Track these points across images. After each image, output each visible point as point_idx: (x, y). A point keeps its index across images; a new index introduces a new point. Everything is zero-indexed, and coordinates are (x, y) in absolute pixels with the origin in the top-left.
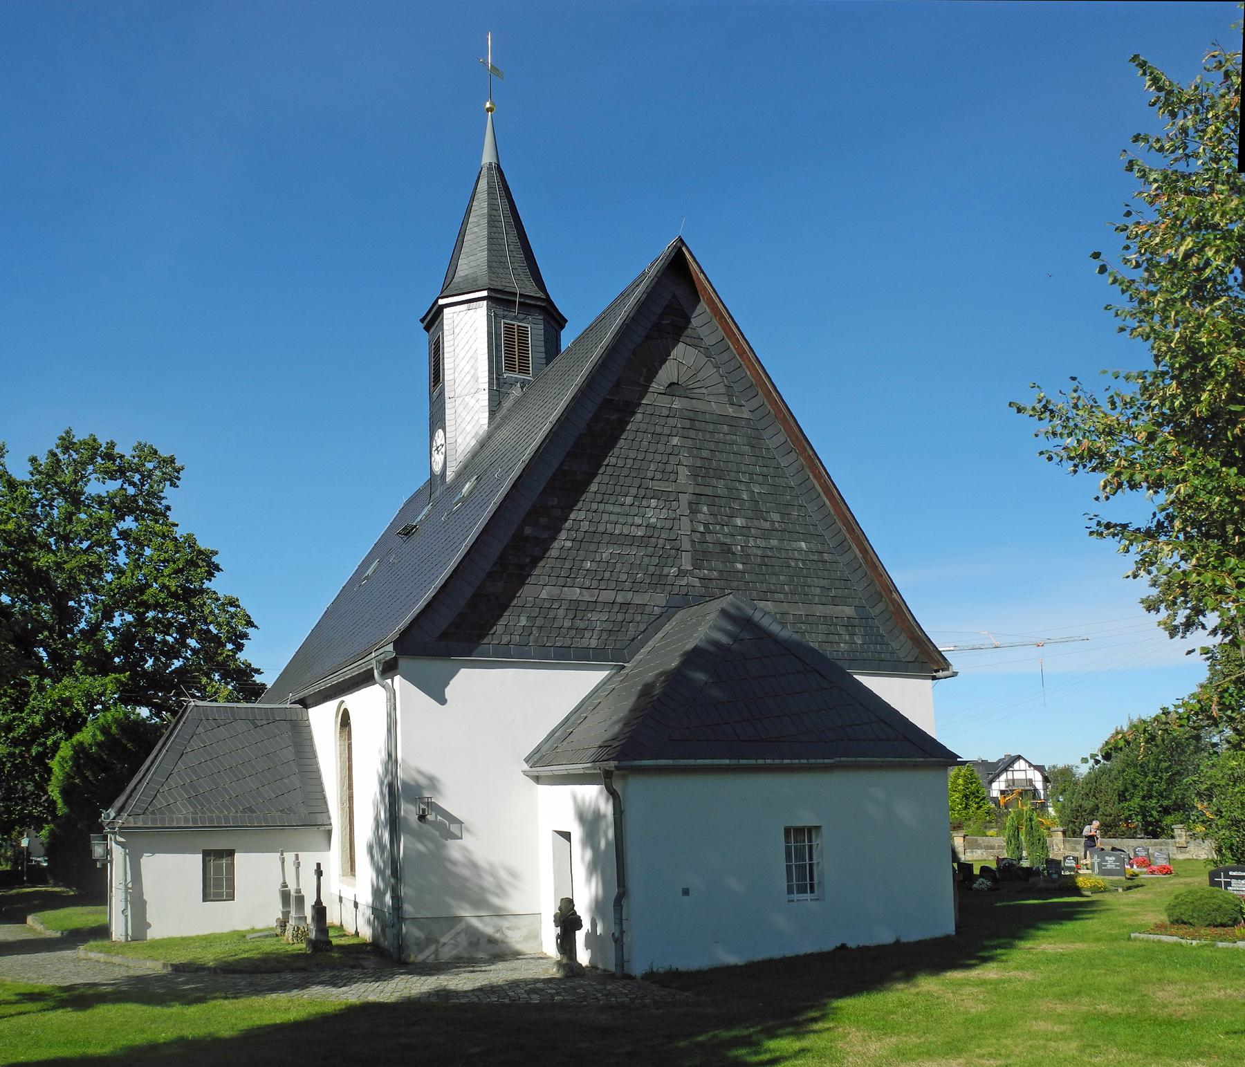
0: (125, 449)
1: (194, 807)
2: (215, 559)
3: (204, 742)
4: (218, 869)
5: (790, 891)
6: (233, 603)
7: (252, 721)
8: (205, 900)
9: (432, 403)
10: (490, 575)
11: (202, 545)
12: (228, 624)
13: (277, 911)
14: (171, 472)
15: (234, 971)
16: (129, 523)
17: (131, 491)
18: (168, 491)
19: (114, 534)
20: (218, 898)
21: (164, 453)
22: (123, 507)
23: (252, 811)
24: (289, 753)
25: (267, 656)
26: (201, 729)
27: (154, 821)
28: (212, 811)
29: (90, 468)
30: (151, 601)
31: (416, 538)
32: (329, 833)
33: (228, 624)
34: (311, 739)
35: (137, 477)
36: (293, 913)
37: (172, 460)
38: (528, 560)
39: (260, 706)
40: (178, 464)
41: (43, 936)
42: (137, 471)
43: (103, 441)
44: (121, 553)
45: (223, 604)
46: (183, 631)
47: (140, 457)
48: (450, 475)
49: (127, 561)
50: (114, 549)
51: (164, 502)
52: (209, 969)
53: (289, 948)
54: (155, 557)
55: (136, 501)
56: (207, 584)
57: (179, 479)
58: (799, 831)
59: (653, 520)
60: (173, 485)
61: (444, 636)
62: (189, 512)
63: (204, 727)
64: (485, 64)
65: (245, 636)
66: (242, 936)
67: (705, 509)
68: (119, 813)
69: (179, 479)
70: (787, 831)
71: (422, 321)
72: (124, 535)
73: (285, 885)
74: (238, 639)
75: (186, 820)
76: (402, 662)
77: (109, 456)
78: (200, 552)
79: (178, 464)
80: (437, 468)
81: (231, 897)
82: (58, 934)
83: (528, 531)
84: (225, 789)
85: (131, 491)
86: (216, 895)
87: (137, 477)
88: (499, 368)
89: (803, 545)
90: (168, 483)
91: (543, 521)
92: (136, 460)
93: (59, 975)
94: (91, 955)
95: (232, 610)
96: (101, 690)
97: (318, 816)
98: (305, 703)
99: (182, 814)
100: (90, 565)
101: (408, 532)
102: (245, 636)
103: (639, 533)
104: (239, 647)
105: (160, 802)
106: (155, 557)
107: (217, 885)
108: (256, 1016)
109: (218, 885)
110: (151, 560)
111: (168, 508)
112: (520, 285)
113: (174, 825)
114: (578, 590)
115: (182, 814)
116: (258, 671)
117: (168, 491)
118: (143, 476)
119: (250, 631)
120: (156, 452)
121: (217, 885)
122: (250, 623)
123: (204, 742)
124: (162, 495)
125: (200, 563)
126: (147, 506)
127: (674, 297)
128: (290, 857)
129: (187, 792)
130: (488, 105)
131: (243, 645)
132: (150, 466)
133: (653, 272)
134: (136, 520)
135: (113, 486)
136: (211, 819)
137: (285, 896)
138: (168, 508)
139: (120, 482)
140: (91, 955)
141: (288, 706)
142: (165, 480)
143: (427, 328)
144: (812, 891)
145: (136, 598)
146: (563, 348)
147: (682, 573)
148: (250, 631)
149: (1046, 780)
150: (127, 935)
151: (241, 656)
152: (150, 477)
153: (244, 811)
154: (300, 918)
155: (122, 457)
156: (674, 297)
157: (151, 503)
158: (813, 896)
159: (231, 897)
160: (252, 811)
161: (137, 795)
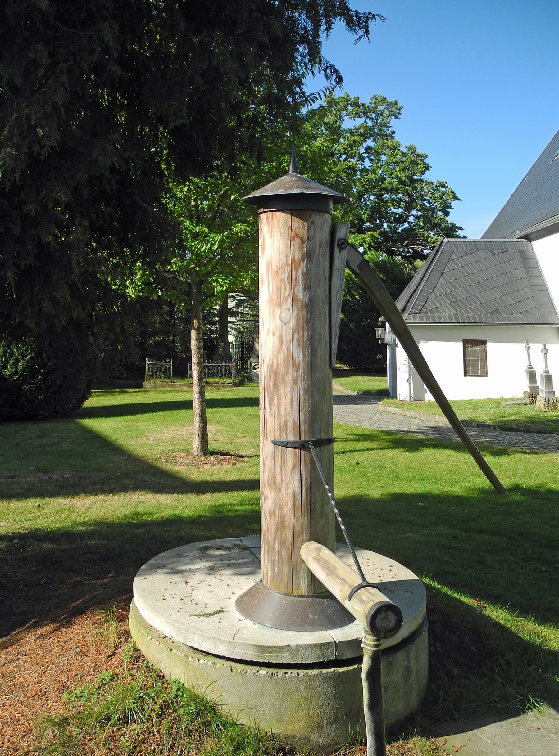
0: (366, 100)
1: (455, 309)
2: (426, 161)
3: (456, 264)
4: (475, 354)
6: (443, 185)
7: (491, 251)
8: (465, 375)
11: (419, 151)
12: (441, 198)
13: (525, 386)
14: (395, 110)
15: (511, 430)
16: (370, 143)
17: (370, 123)
18: (393, 122)
19: (362, 150)
21: (390, 99)
22: (366, 134)
23: (499, 313)
24: (520, 273)
26: (454, 256)
27: (427, 318)
28: (468, 312)
29: (344, 113)
30: (389, 188)
33: (441, 198)
34: (536, 262)
35: (374, 115)
37: (396, 103)
40: (399, 105)
41: (343, 394)
42: (374, 112)
43: (352, 96)
44: (367, 160)
45: (437, 186)
46: (409, 207)
47: (375, 103)
49: (371, 165)
50: (362, 159)
51: (391, 129)
52: (489, 426)
53: (541, 415)
54: (390, 161)
55: (373, 130)
56: (424, 177)
57: (400, 114)
60: (397, 118)
62: (406, 133)
63: (456, 255)
65: (450, 207)
66: (498, 402)
69: (400, 114)
72: (368, 150)
73: (530, 367)
74: (446, 208)
75: (451, 318)
77: (356, 104)
78: (419, 155)
79: (399, 105)
81: (485, 374)
82: (356, 393)
84: (476, 297)
85: (370, 123)
86: (473, 372)
87: (374, 115)
90: (393, 117)
92: (373, 105)
94: (390, 409)
95: (443, 189)
96: (361, 242)
97: (550, 317)
98: (528, 238)
99: (447, 314)
100: (349, 167)
102: (450, 207)
104: (447, 214)
105: (430, 306)
106: (390, 161)
107: (474, 366)
108: (183, 397)
109: (475, 366)
110: (387, 163)
111: (393, 132)
113: (442, 321)
115: (447, 314)
116: (460, 228)
117: (393, 122)
118: (377, 114)
119: (454, 203)
120: (385, 99)
121: (474, 366)
122: (455, 198)
123: (456, 264)
124: (389, 125)
125: (419, 162)
126: (381, 133)
128: (536, 348)
129: (449, 299)
131: (449, 212)
132: (381, 108)
134: (374, 140)
135: (359, 122)
136: (468, 318)
138: (393, 132)
139: (364, 119)
140: (390, 409)
141: (516, 240)
142: (391, 115)
145: (380, 186)
148: (454, 203)
150: (411, 397)
151: (449, 219)
152: (381, 114)
153: (492, 312)
154: (550, 392)
155: (364, 105)
157: (382, 130)
159: (485, 374)
160: (499, 313)
161: (414, 300)
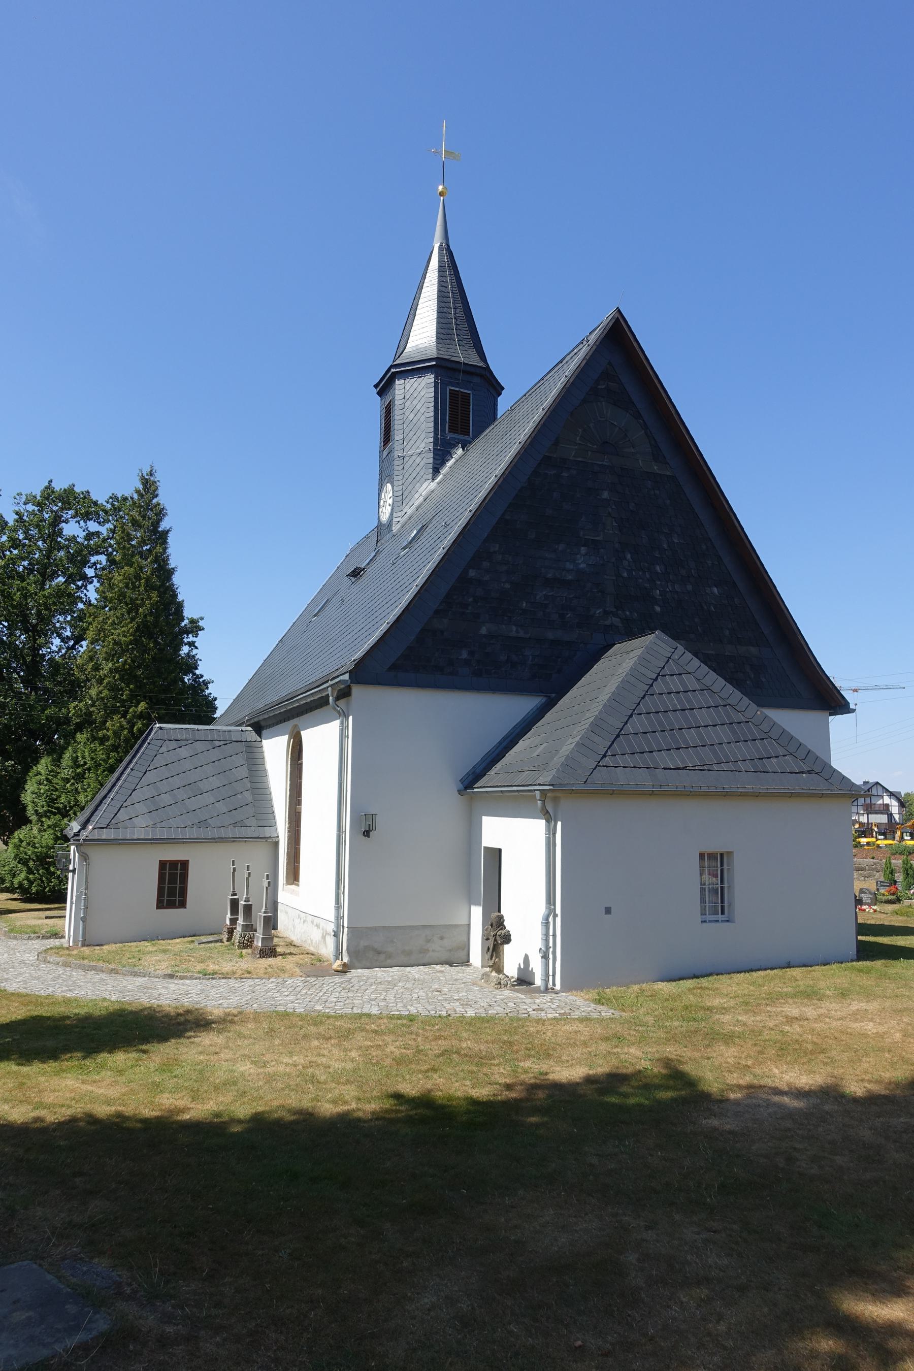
5: (703, 913)
9: (382, 461)
10: (437, 612)
18: (194, 652)
20: (171, 905)
24: (243, 772)
25: (226, 664)
31: (365, 578)
32: (276, 844)
36: (240, 921)
38: (471, 600)
39: (219, 728)
48: (395, 528)
58: (712, 856)
59: (582, 566)
61: (394, 667)
64: (438, 153)
67: (629, 556)
68: (84, 826)
70: (702, 856)
71: (376, 386)
76: (356, 690)
80: (384, 518)
83: (472, 573)
88: (443, 431)
89: (715, 590)
91: (486, 564)
93: (20, 979)
101: (356, 573)
103: (570, 577)
112: (463, 355)
114: (514, 628)
127: (610, 363)
130: (440, 188)
133: (593, 338)
137: (234, 904)
143: (380, 394)
144: (723, 913)
146: (500, 412)
147: (606, 613)
149: (902, 804)
156: (610, 363)
158: (724, 917)
